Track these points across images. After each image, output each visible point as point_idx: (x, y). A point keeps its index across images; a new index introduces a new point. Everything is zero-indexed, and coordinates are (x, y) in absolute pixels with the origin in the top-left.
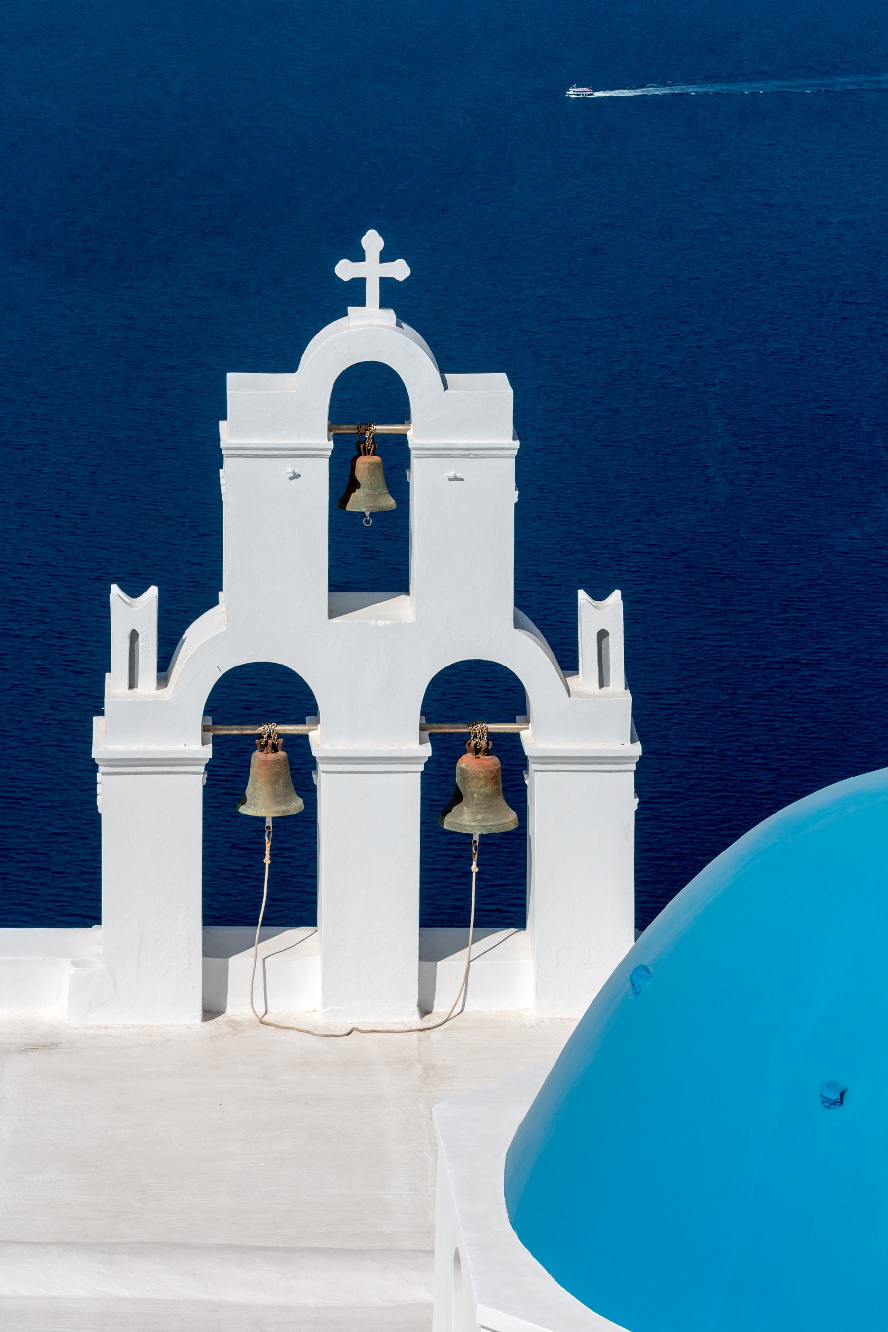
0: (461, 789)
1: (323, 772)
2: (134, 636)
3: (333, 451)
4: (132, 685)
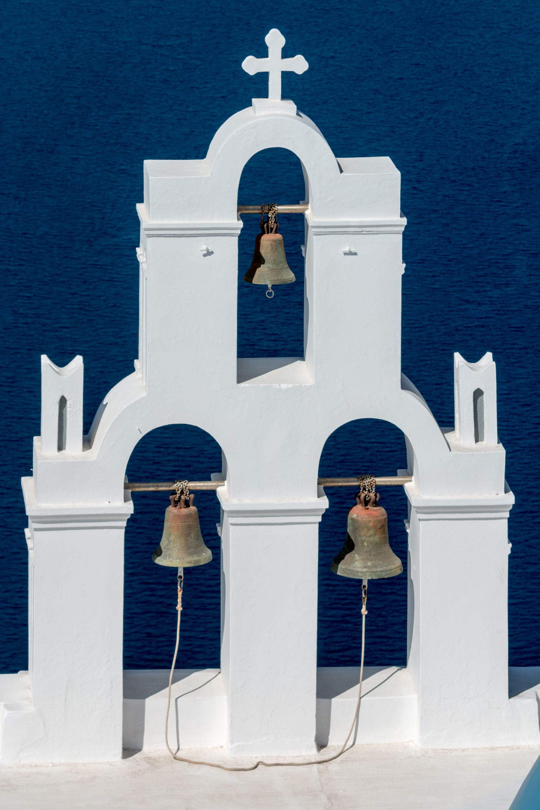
0: (353, 538)
1: (232, 524)
2: (63, 402)
4: (61, 447)
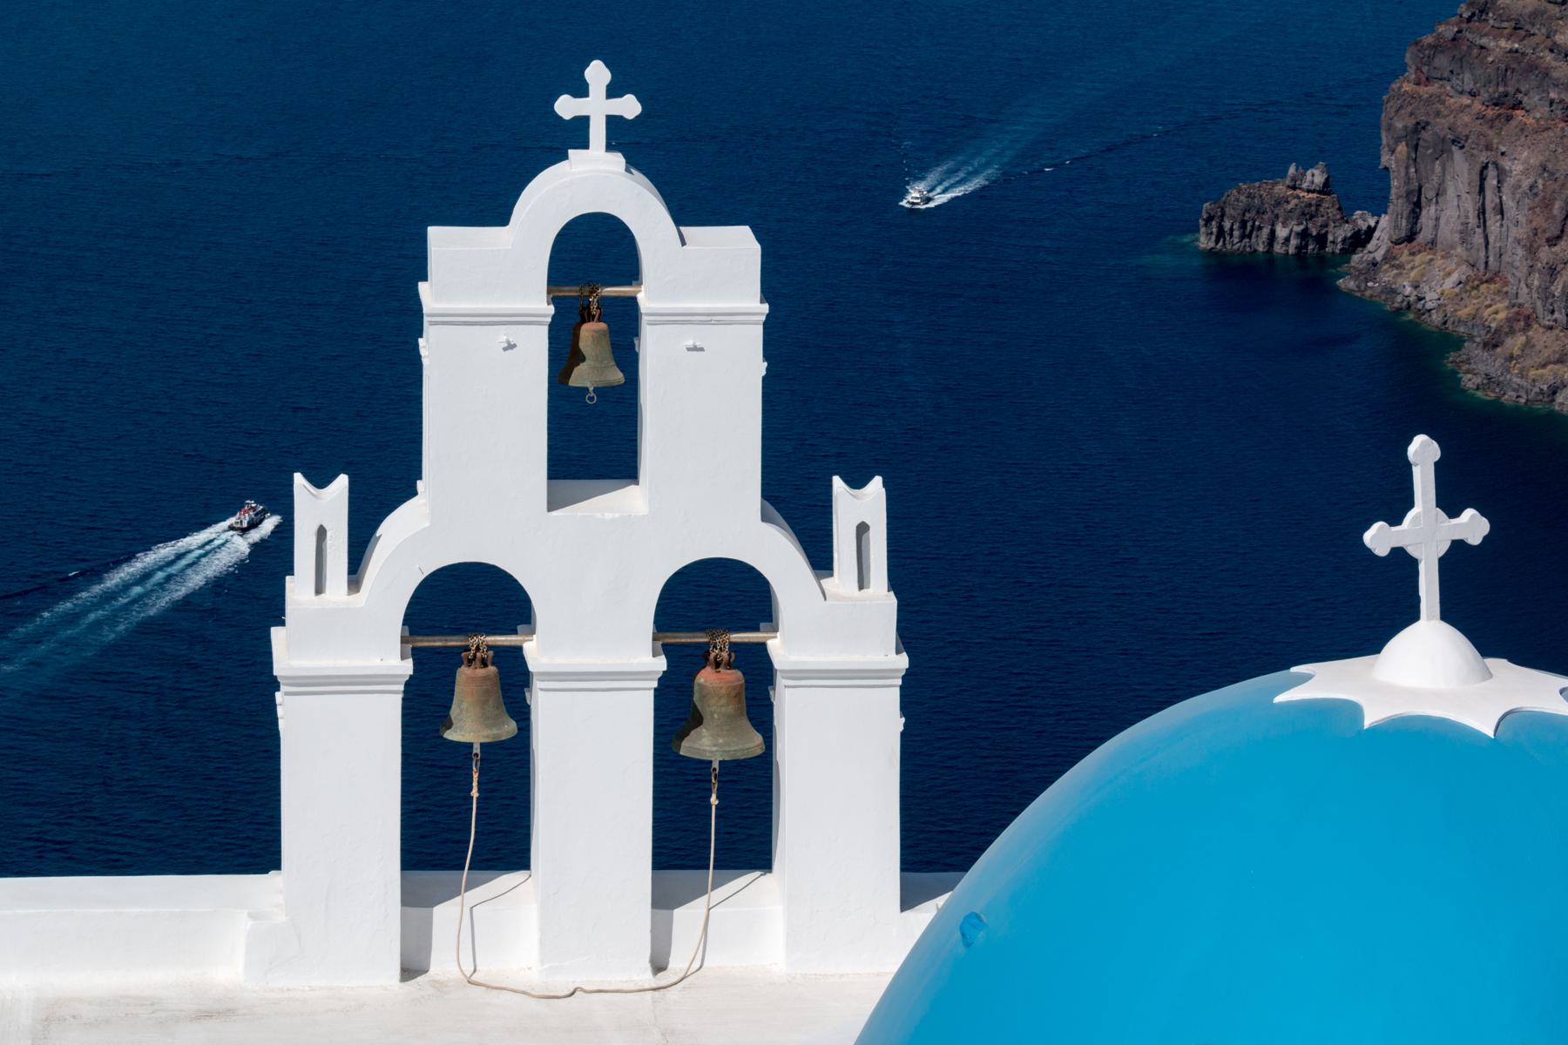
2: (321, 533)
3: (554, 317)
4: (319, 590)
